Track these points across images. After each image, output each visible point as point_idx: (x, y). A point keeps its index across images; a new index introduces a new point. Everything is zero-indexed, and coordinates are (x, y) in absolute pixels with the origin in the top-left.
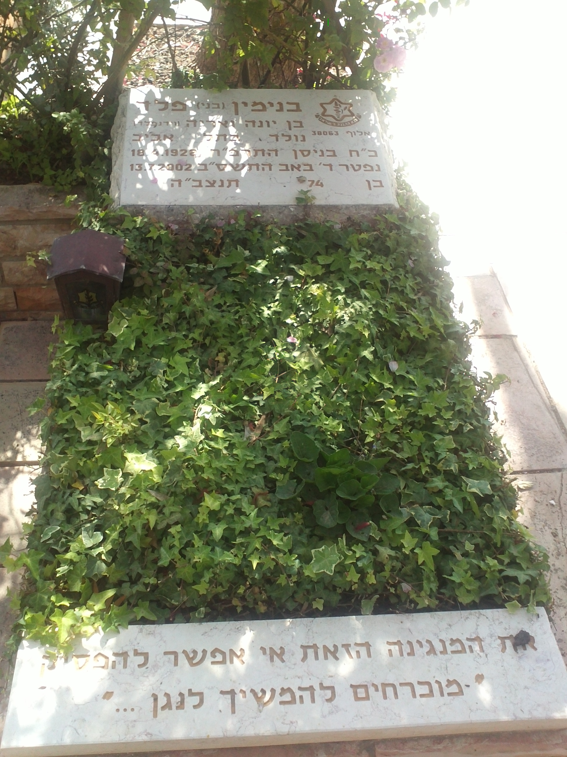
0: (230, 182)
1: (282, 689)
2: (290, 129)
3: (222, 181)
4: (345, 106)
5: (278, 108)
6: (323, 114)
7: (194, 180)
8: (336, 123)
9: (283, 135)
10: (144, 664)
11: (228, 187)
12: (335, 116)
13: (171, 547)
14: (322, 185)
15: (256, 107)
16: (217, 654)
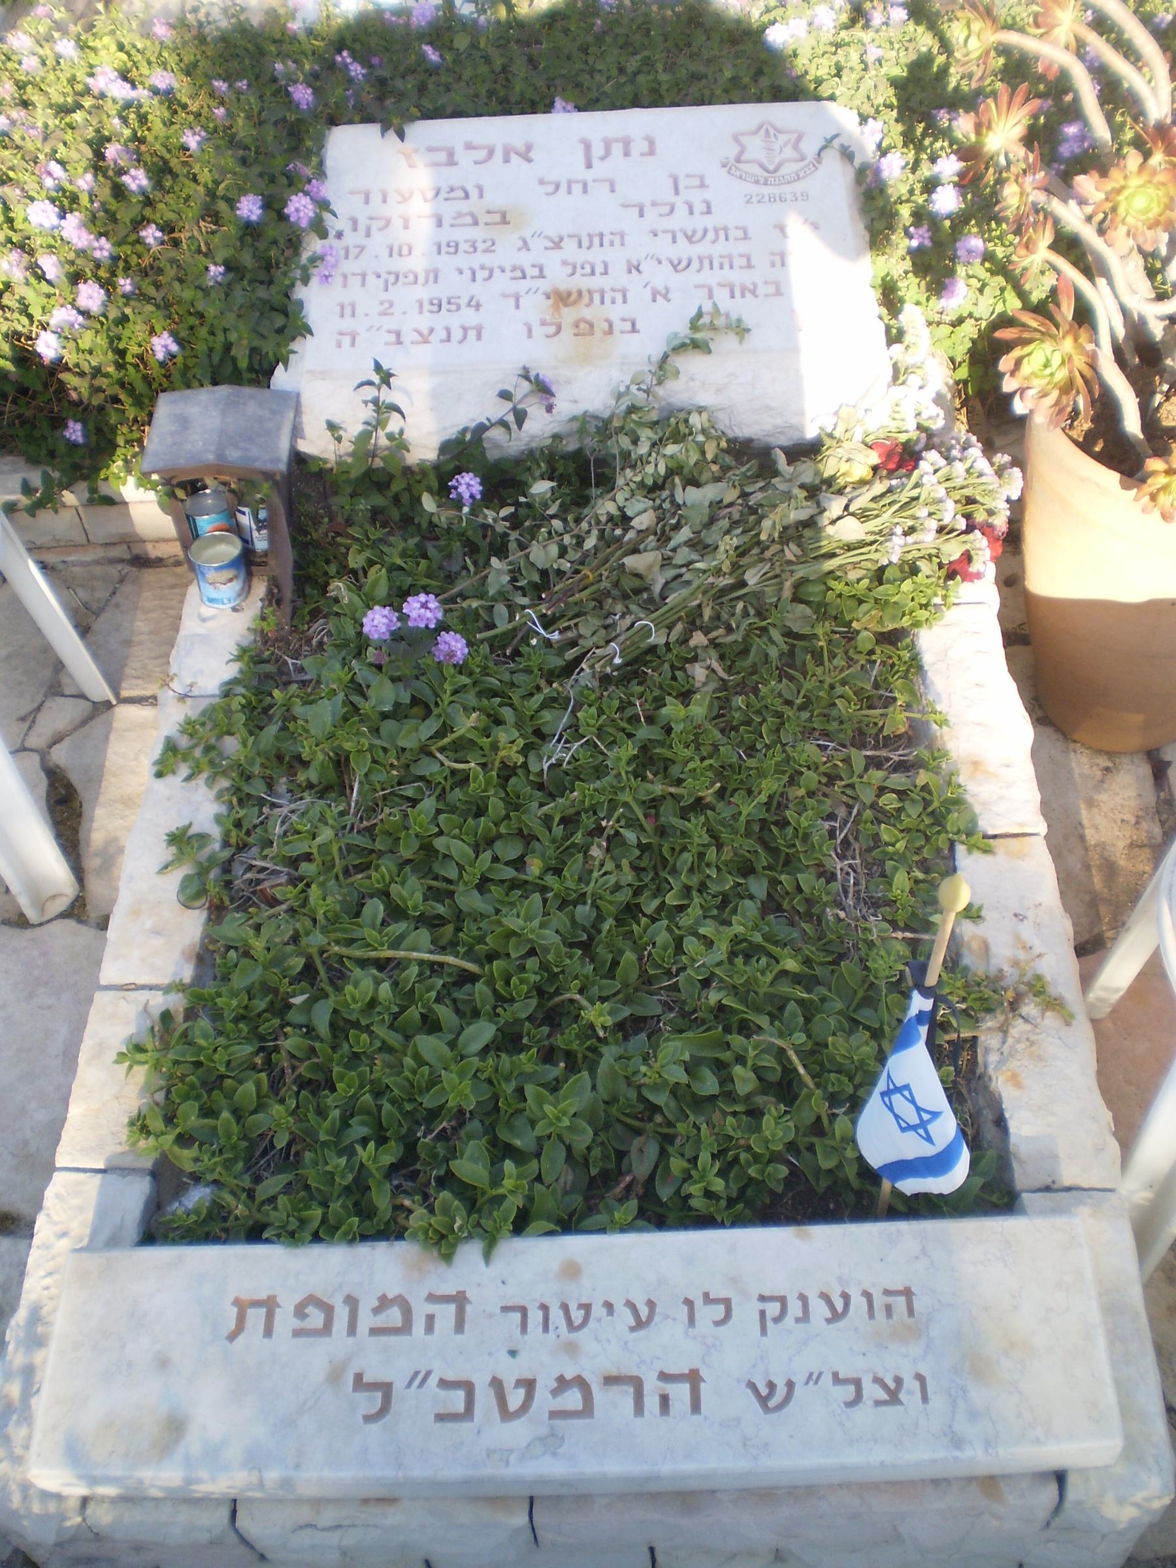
1: (561, 1379)
5: (646, 149)
6: (738, 160)
9: (654, 204)
12: (765, 162)
15: (452, 195)
16: (310, 1310)
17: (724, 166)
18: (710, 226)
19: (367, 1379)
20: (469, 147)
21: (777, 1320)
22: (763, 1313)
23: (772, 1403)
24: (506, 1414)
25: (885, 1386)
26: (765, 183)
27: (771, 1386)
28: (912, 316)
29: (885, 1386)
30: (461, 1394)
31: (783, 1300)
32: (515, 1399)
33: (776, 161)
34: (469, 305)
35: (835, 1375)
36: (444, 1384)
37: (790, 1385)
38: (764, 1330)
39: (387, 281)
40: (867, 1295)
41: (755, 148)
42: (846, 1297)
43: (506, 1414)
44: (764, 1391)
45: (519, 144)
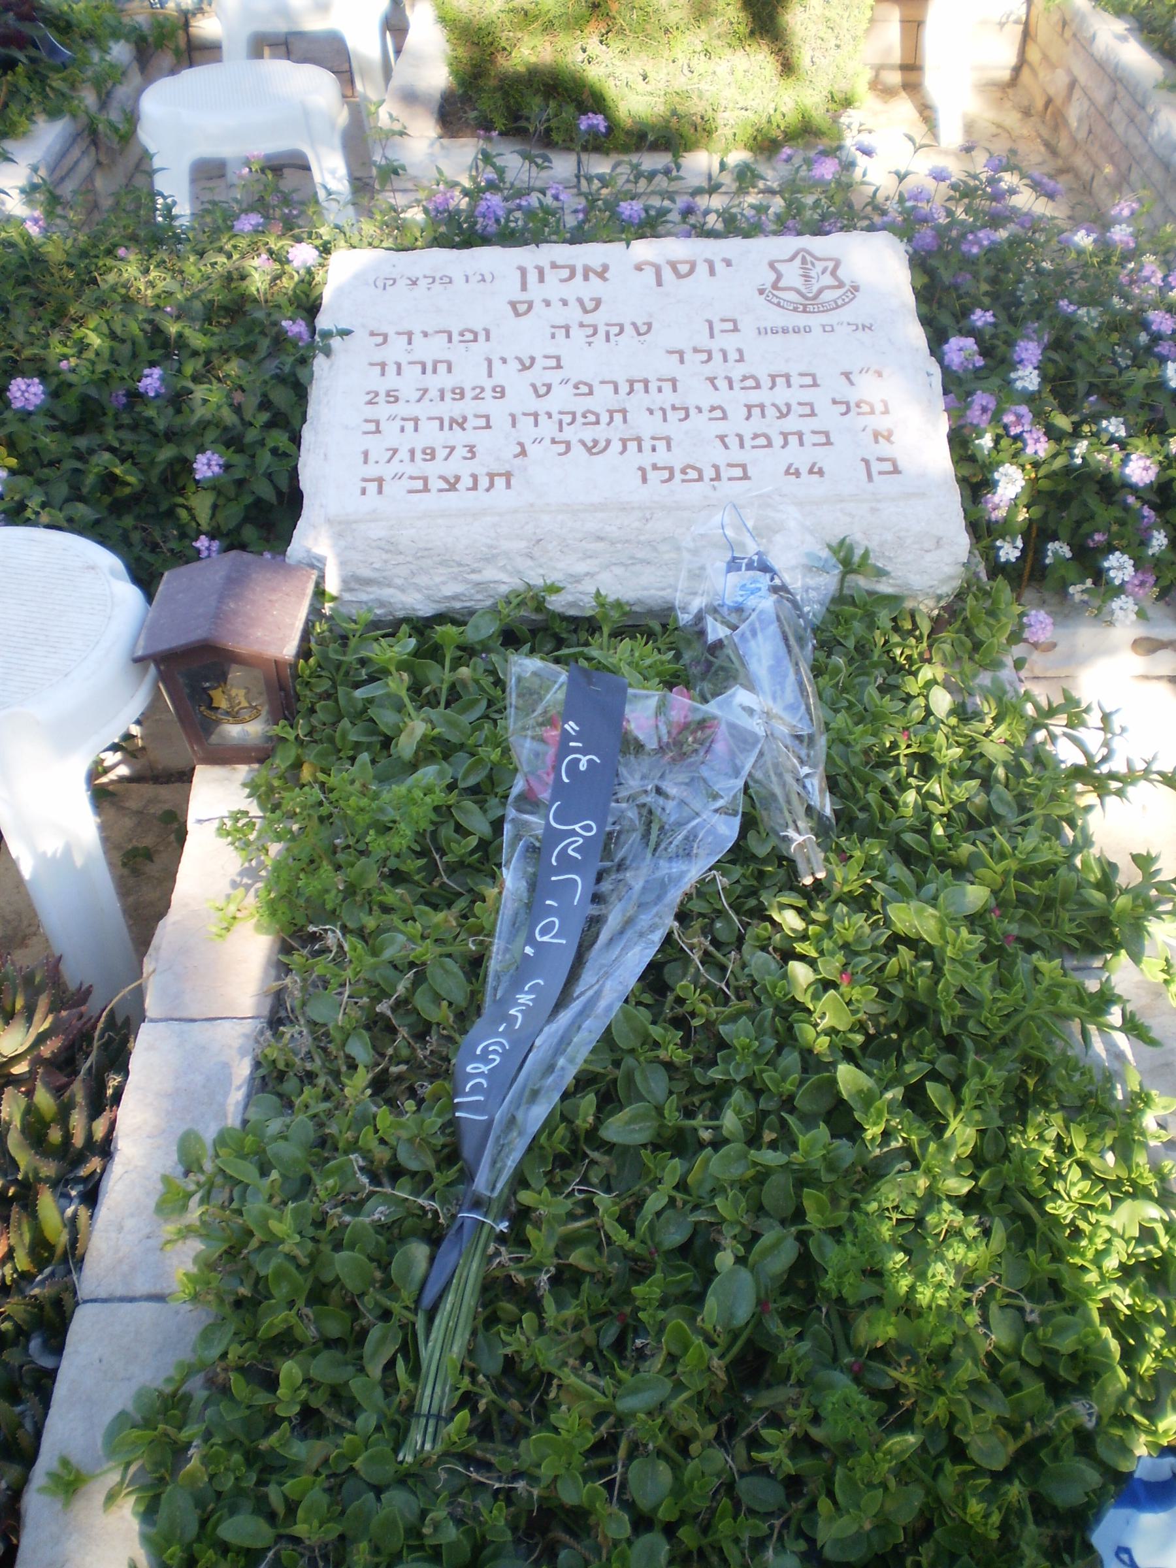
0: (491, 476)
2: (712, 336)
3: (475, 478)
6: (775, 286)
7: (411, 478)
8: (805, 306)
10: (566, 453)
11: (488, 490)
12: (803, 290)
13: (337, 1446)
14: (821, 473)
17: (761, 292)
18: (481, 471)
20: (554, 266)
26: (804, 311)
28: (480, 1336)
31: (574, 414)
33: (815, 289)
34: (811, 472)
39: (561, 422)
41: (792, 275)
45: (596, 264)
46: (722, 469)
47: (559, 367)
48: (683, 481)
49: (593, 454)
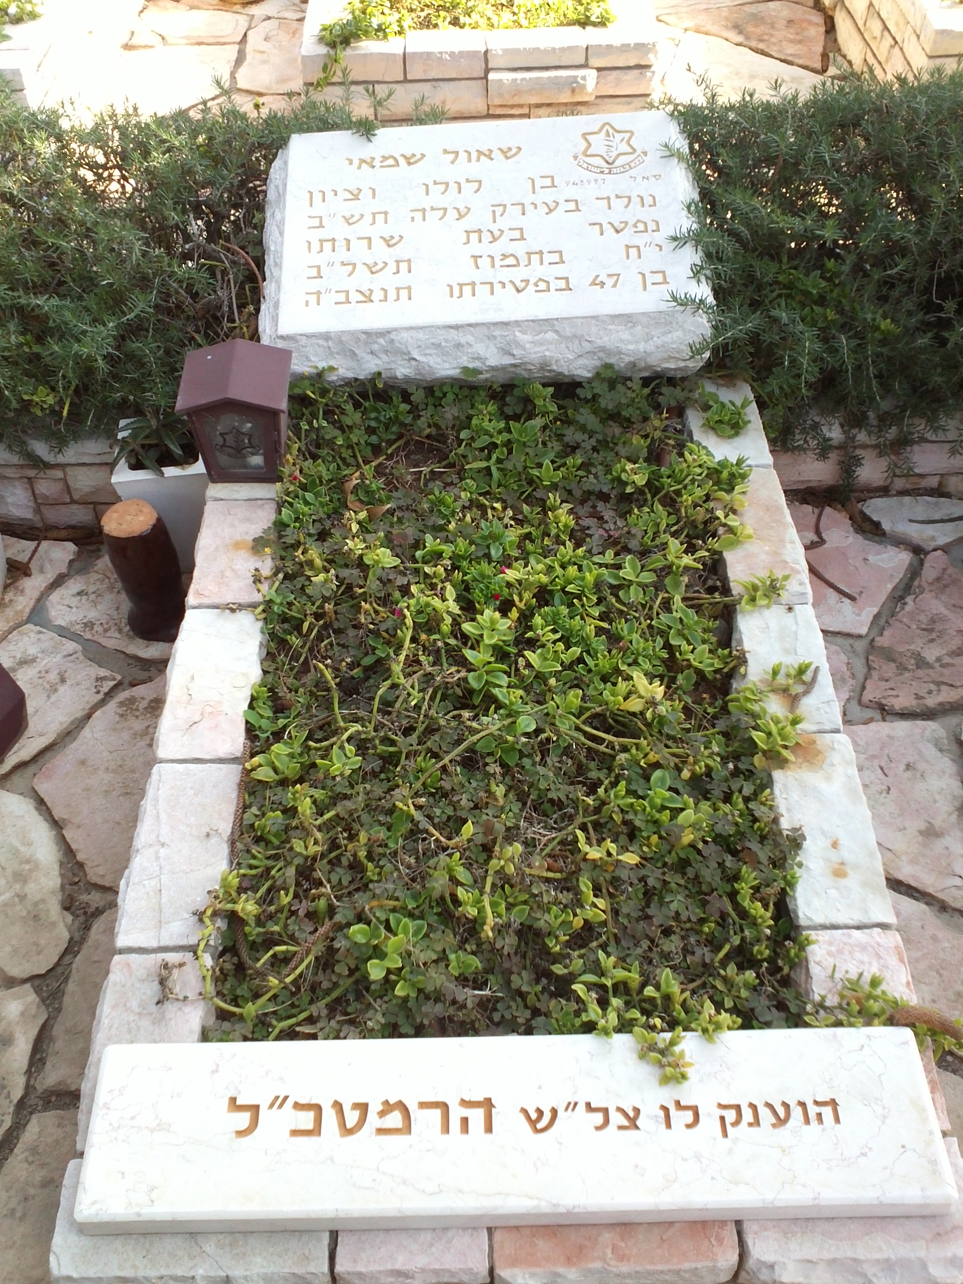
4: (622, 135)
19: (239, 1102)
21: (736, 1123)
22: (722, 1119)
23: (540, 1126)
24: (346, 1131)
25: (626, 1115)
27: (540, 1113)
29: (626, 1115)
30: (311, 1115)
31: (738, 1108)
32: (352, 1118)
35: (588, 1105)
36: (297, 1106)
37: (554, 1112)
38: (725, 1134)
40: (802, 1105)
42: (786, 1106)
43: (346, 1131)
44: (534, 1116)
46: (648, 275)
47: (522, 238)
48: (381, 1131)
49: (350, 224)
